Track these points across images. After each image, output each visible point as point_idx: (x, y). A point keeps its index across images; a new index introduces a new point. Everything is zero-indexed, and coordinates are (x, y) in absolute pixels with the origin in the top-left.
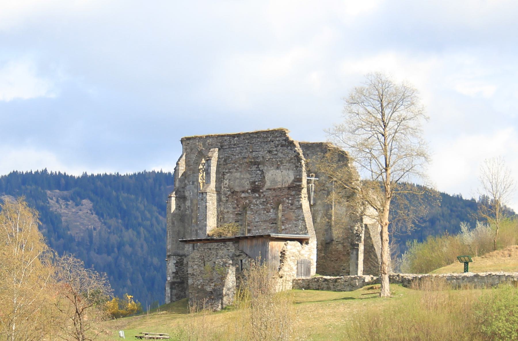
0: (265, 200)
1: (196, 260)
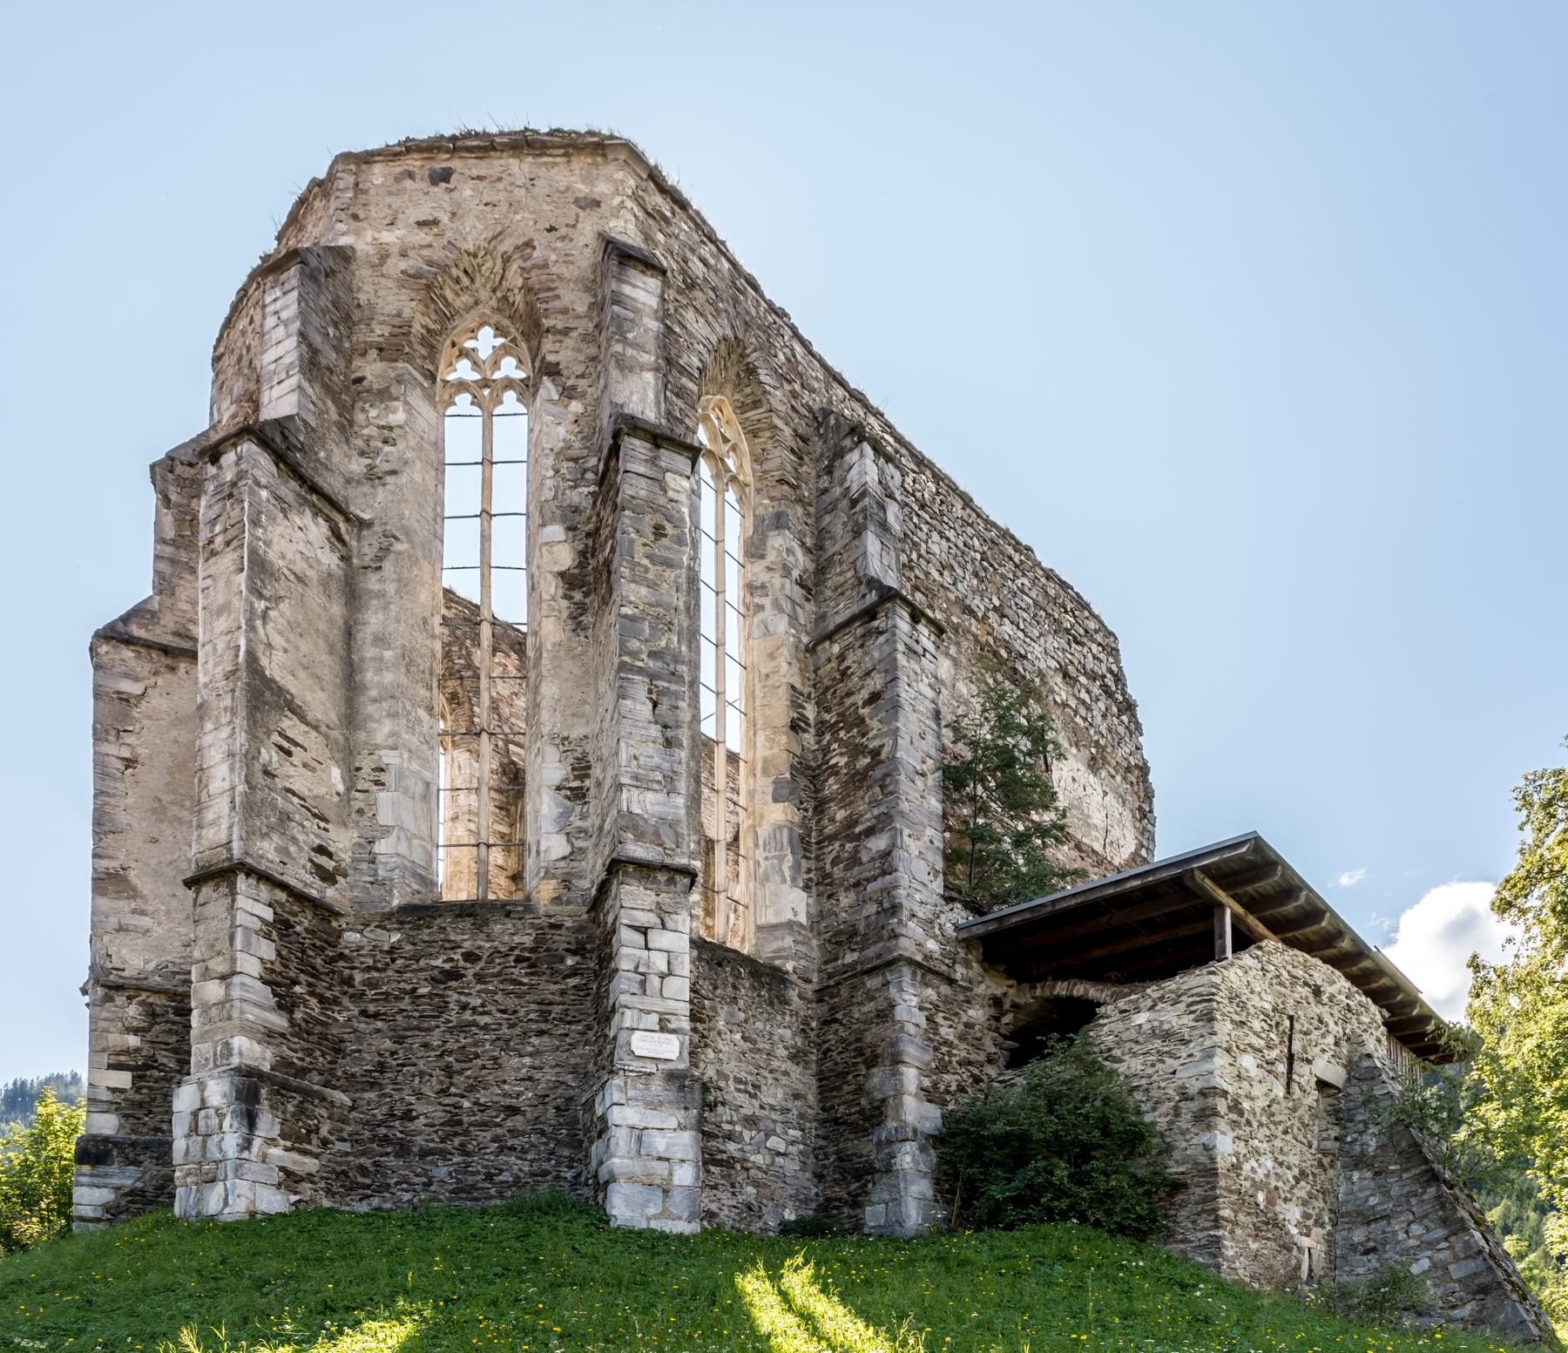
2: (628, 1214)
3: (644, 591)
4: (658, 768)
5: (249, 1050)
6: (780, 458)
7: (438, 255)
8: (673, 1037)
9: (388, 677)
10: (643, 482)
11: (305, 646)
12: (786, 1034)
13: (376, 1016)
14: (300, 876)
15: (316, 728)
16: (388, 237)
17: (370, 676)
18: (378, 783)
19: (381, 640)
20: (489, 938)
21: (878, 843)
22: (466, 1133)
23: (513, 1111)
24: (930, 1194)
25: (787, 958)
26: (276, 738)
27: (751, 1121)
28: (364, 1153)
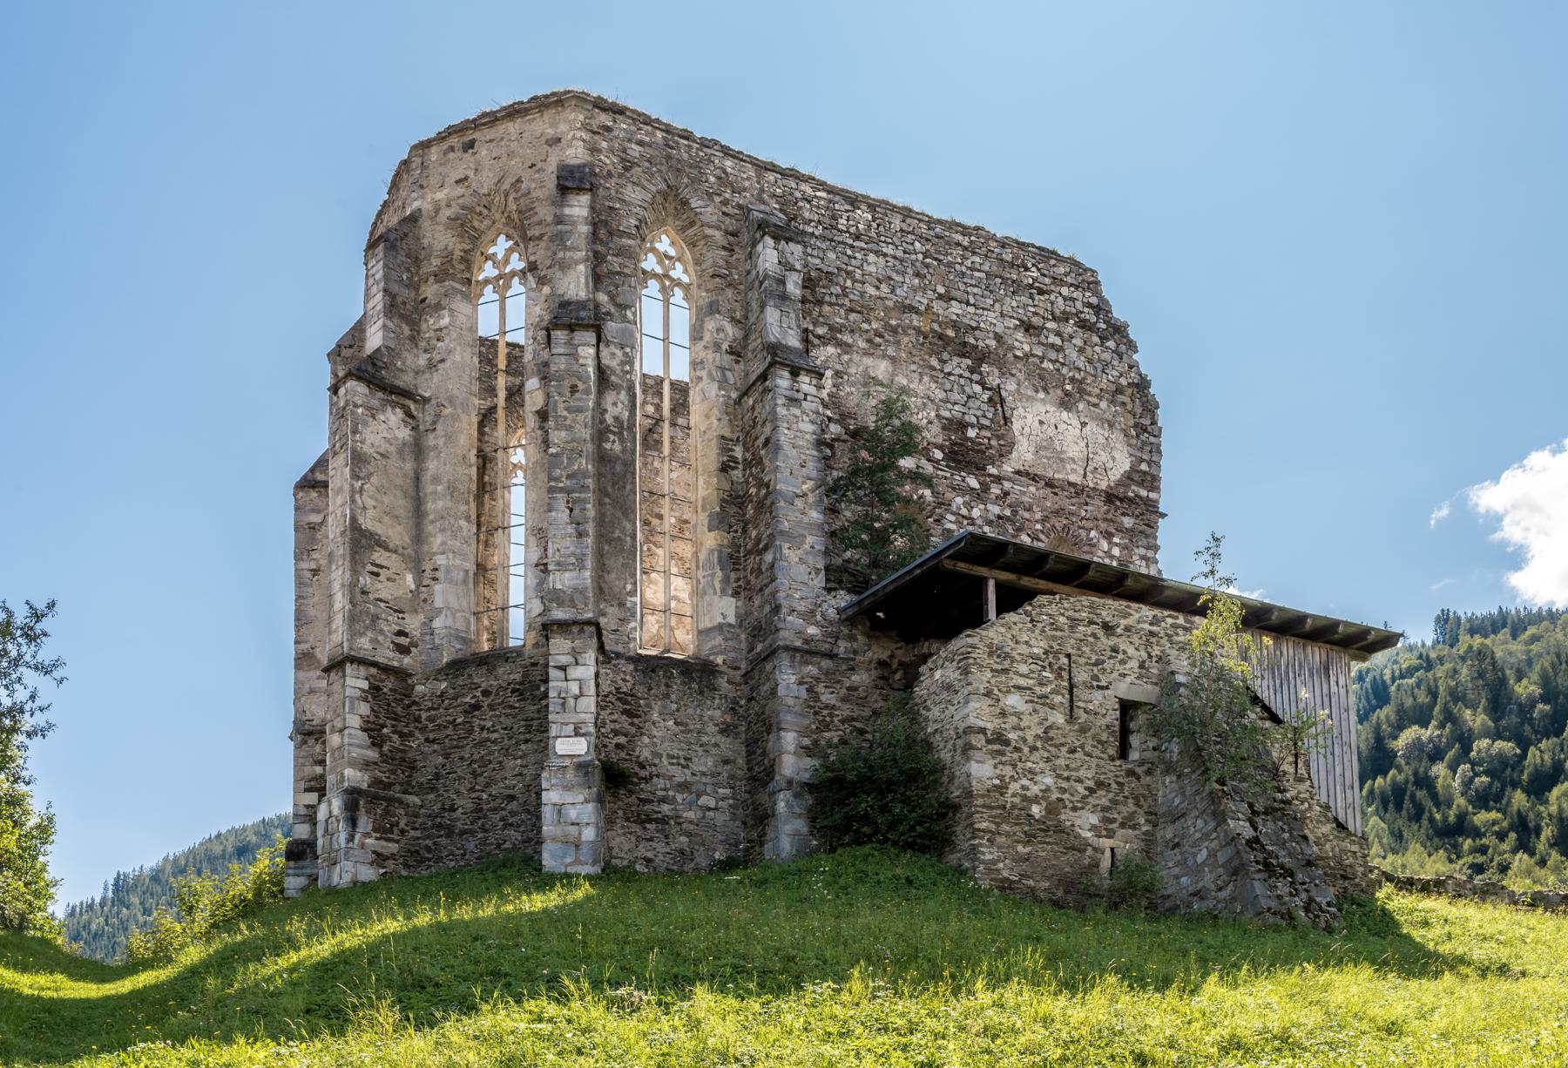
0: (1008, 512)
1: (1024, 669)
2: (553, 863)
3: (563, 434)
4: (573, 554)
5: (355, 777)
6: (715, 257)
7: (467, 201)
8: (582, 739)
9: (440, 504)
10: (563, 359)
11: (387, 500)
12: (715, 713)
13: (433, 741)
14: (386, 655)
15: (395, 552)
16: (440, 195)
17: (430, 506)
18: (435, 579)
19: (436, 480)
20: (496, 679)
21: (768, 557)
22: (485, 816)
23: (512, 798)
24: (805, 830)
25: (716, 654)
26: (370, 568)
27: (684, 787)
28: (428, 837)
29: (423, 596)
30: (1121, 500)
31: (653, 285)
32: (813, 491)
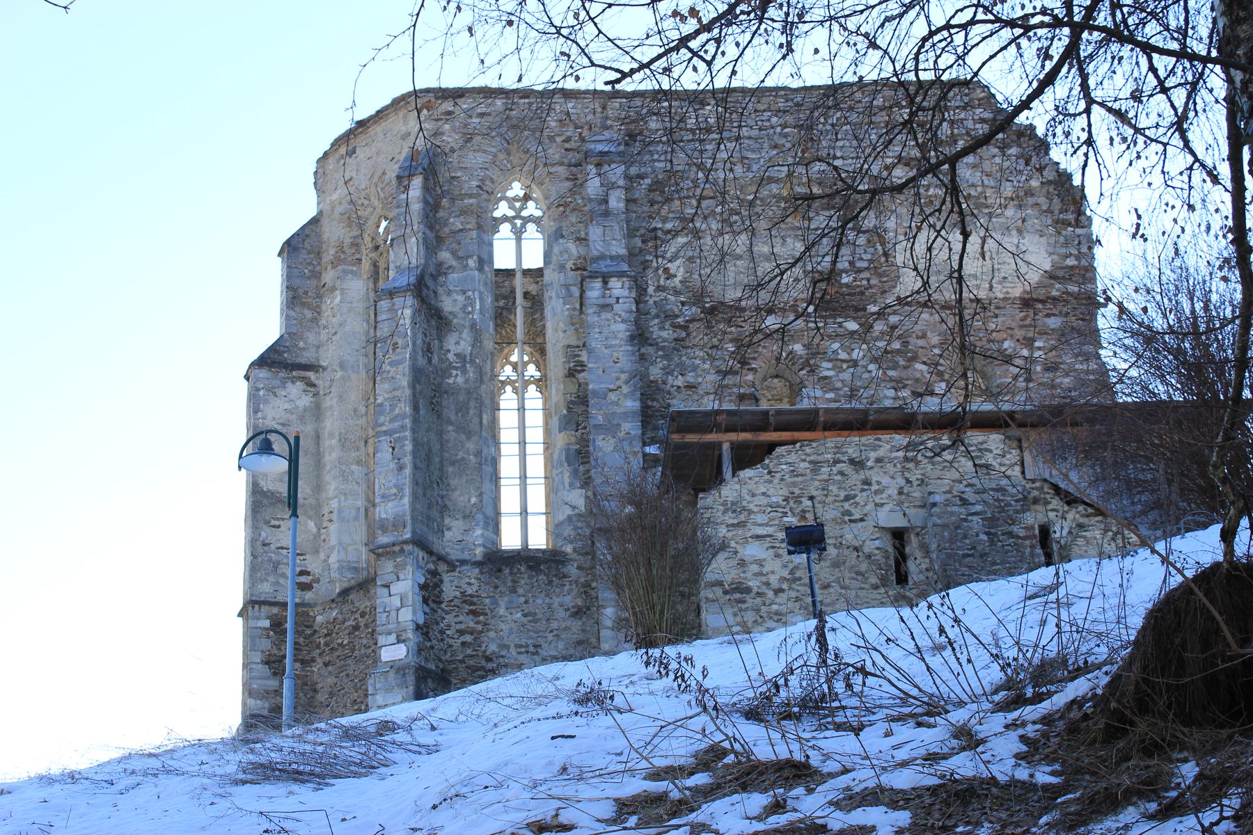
1: (760, 518)
18: (331, 521)
29: (323, 537)
30: (1042, 301)
31: (505, 228)
32: (627, 383)
